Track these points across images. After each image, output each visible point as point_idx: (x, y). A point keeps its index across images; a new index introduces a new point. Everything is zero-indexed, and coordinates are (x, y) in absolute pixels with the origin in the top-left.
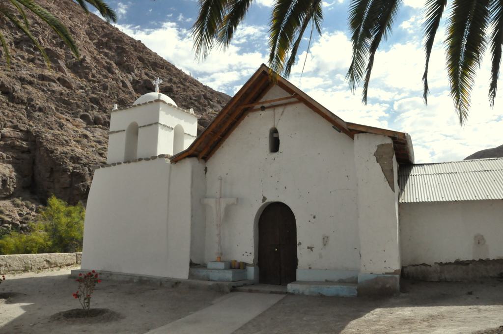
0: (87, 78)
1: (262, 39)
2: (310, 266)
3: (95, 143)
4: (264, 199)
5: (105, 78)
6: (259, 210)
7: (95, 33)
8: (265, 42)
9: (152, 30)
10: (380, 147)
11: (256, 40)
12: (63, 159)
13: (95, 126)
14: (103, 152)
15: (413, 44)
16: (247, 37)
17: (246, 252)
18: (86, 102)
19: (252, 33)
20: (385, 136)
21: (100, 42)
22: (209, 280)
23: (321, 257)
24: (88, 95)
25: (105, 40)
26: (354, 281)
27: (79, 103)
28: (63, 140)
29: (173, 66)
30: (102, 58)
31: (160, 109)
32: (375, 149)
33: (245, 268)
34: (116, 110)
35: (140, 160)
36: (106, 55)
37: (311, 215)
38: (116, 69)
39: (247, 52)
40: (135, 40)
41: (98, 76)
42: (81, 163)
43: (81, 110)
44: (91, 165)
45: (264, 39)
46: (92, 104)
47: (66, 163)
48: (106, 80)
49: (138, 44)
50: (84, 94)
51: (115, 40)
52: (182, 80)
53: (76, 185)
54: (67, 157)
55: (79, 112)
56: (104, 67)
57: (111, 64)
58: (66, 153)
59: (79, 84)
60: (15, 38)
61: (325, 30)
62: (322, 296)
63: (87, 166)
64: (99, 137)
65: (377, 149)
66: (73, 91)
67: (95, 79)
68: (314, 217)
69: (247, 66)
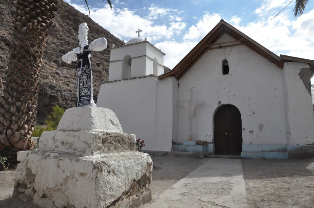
0: (57, 37)
1: (167, 17)
2: (251, 143)
3: (63, 78)
4: (220, 102)
5: (68, 38)
6: (217, 108)
7: (60, 10)
8: (169, 19)
9: (97, 9)
10: (302, 70)
11: (164, 17)
12: (45, 87)
13: (63, 67)
14: (69, 83)
15: (262, 23)
16: (158, 15)
17: (208, 135)
18: (57, 52)
19: (161, 13)
20: (305, 63)
21: (64, 15)
22: (186, 152)
23: (258, 137)
24: (58, 48)
25: (66, 14)
26: (284, 150)
27: (53, 52)
28: (44, 75)
29: (109, 32)
30: (65, 25)
31: (147, 47)
32: (299, 71)
33: (207, 145)
34: (114, 48)
35: (135, 78)
36: (67, 23)
37: (251, 112)
38: (74, 32)
39: (157, 25)
40: (85, 15)
41: (64, 36)
42: (56, 90)
43: (54, 57)
44: (62, 91)
45: (169, 17)
46: (61, 54)
47: (46, 89)
48: (68, 39)
49: (87, 17)
50: (55, 47)
51: (73, 14)
52: (114, 41)
53: (53, 104)
54: (47, 86)
55: (53, 58)
56: (67, 31)
57: (71, 29)
58: (46, 83)
59: (52, 41)
60: (11, 10)
61: (208, 12)
62: (264, 159)
63: (60, 92)
64: (65, 74)
65: (300, 71)
66: (48, 45)
67: (62, 38)
68: (254, 113)
69: (157, 34)
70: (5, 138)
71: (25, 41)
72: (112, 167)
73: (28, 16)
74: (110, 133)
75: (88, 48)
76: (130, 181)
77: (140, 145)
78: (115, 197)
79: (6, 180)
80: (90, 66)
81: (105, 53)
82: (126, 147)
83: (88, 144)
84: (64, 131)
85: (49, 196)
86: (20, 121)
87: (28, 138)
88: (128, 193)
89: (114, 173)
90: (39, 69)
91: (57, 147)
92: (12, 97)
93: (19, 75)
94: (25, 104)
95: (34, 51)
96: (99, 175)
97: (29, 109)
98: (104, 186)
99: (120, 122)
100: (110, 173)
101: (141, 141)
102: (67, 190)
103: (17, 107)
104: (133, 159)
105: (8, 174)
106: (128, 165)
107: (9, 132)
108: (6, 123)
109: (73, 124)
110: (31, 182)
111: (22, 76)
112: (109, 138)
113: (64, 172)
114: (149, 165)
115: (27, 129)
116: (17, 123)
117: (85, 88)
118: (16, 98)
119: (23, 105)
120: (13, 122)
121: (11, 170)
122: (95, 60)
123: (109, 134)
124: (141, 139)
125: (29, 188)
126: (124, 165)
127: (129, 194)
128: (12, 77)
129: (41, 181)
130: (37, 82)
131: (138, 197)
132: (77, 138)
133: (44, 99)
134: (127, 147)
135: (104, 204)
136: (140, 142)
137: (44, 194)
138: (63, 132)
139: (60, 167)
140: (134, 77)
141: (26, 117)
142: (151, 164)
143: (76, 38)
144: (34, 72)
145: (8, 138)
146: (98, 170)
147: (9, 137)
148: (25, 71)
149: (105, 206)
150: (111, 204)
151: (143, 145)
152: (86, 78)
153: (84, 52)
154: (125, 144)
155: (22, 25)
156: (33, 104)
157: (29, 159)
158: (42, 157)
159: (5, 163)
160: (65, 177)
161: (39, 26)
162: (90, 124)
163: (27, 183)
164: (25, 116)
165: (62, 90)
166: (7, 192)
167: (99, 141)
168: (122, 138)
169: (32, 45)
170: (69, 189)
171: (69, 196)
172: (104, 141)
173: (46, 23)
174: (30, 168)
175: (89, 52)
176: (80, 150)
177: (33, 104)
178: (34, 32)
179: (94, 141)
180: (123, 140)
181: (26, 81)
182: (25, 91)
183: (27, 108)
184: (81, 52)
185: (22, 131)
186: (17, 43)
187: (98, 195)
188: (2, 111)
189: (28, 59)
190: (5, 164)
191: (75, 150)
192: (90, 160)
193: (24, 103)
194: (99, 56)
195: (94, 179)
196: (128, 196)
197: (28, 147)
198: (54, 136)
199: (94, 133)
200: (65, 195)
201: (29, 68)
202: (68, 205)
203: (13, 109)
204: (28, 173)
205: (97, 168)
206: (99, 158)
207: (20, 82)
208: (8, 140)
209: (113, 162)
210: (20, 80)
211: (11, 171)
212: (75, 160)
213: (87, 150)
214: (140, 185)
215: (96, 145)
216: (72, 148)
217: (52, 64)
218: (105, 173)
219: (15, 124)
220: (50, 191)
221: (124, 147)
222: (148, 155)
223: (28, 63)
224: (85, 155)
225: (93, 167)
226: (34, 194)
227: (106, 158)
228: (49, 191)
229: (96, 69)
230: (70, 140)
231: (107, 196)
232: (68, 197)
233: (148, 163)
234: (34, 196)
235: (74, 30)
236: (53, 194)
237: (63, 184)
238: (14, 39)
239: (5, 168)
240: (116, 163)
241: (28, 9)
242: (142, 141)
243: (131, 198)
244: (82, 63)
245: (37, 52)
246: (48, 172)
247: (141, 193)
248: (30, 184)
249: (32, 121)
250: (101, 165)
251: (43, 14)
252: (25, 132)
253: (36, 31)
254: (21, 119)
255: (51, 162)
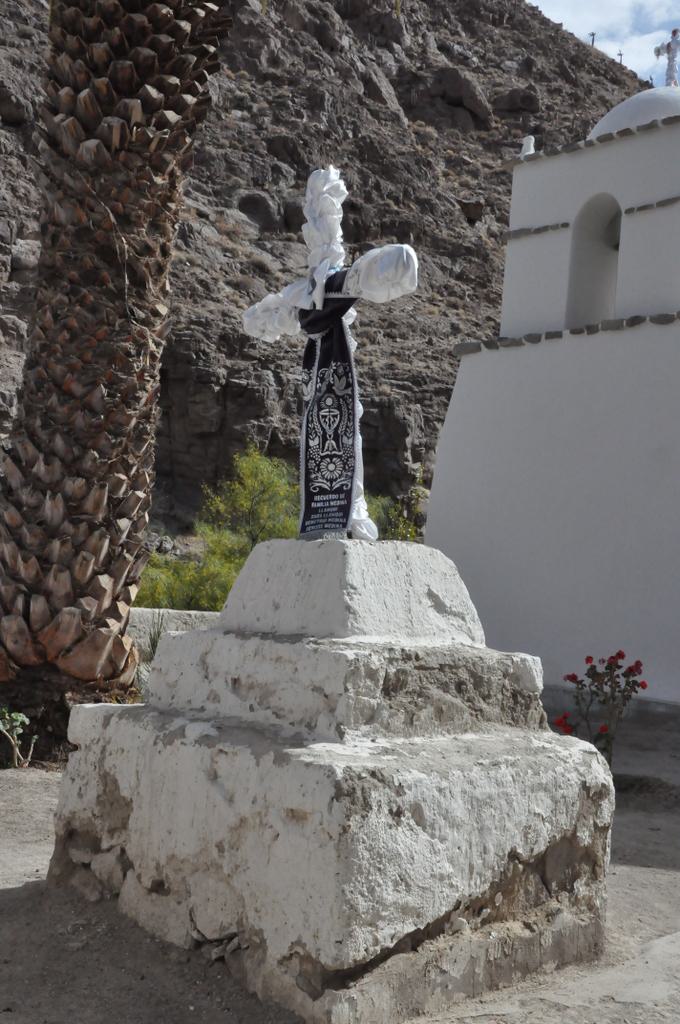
0: (253, 69)
12: (199, 341)
18: (257, 153)
28: (193, 280)
34: (530, 158)
35: (635, 321)
41: (288, 60)
47: (204, 353)
48: (313, 73)
53: (238, 427)
54: (208, 337)
55: (237, 186)
56: (305, 27)
57: (326, 15)
58: (207, 324)
59: (230, 90)
63: (272, 367)
67: (278, 72)
70: (21, 632)
71: (92, 202)
72: (410, 796)
73: (101, 82)
74: (421, 654)
75: (344, 288)
76: (491, 858)
77: (622, 681)
78: (418, 917)
79: (22, 810)
80: (350, 365)
81: (510, 140)
82: (492, 710)
83: (326, 696)
84: (242, 634)
85: (175, 887)
86: (80, 558)
87: (111, 632)
88: (481, 909)
89: (420, 820)
90: (158, 328)
91: (214, 697)
92: (50, 455)
93: (74, 360)
94: (103, 487)
95: (134, 248)
96: (354, 822)
97: (115, 506)
98: (372, 869)
99: (473, 602)
100: (403, 819)
101: (625, 664)
102: (240, 869)
103: (67, 499)
104: (513, 765)
105: (32, 783)
106: (486, 788)
107: (38, 605)
108: (26, 569)
109: (277, 607)
110: (113, 827)
111: (85, 362)
112: (416, 671)
113: (231, 800)
114: (592, 795)
115: (109, 591)
116: (69, 567)
117: (331, 457)
118: (62, 460)
119: (92, 492)
120: (52, 564)
121: (43, 767)
122: (453, 190)
123: (417, 658)
124: (626, 658)
125: (109, 850)
126: (468, 787)
127: (487, 911)
128: (46, 367)
129: (149, 828)
130: (148, 387)
131: (533, 931)
132: (289, 668)
133: (195, 402)
134: (497, 710)
135: (370, 937)
136: (623, 670)
137: (157, 878)
138: (239, 641)
139: (219, 780)
140: (628, 316)
141: (107, 543)
142: (602, 792)
143: (353, 64)
144: (135, 342)
145: (33, 634)
146: (353, 803)
147: (36, 627)
148: (99, 340)
149: (371, 949)
150: (400, 941)
151: (635, 682)
152: (336, 416)
153: (326, 302)
154: (485, 698)
155: (80, 128)
156: (135, 484)
157: (110, 738)
158: (157, 737)
159: (20, 737)
160: (233, 820)
161: (153, 128)
162: (341, 617)
163: (102, 830)
164: (102, 537)
165: (284, 358)
166: (31, 862)
167: (367, 687)
168: (473, 674)
169: (126, 221)
170: (248, 868)
171: (246, 894)
172: (391, 688)
173: (180, 107)
174: (112, 773)
175: (349, 303)
176: (297, 717)
177: (135, 484)
178: (131, 155)
179: (349, 686)
180: (478, 682)
181: (105, 387)
182: (99, 428)
183: (108, 504)
184: (314, 305)
185: (89, 604)
186: (62, 214)
187: (347, 902)
188: (11, 515)
189: (111, 285)
190: (20, 742)
191: (278, 716)
192: (326, 761)
193: (95, 480)
194: (477, 163)
195: (335, 836)
196: (484, 922)
197: (110, 671)
198: (206, 654)
199: (350, 654)
200: (232, 889)
201: (114, 325)
202: (241, 929)
203: (52, 509)
204: (104, 791)
205: (348, 795)
206: (365, 754)
207: (77, 389)
208: (35, 641)
209: (417, 774)
210: (78, 380)
211: (43, 772)
212: (272, 758)
213: (322, 721)
214: (545, 882)
215: (357, 701)
216: (269, 708)
217: (232, 221)
218: (379, 819)
219: (61, 571)
220: (180, 870)
221: (481, 710)
222: (591, 753)
223: (111, 305)
224: (315, 741)
225: (332, 791)
226: (125, 875)
227: (389, 757)
228: (178, 871)
229: (459, 236)
230: (265, 673)
231: (386, 907)
232: (241, 899)
233: (585, 786)
234: (122, 884)
235: (343, 17)
236: (191, 881)
237: (226, 847)
238: (49, 196)
239: (19, 759)
240: (430, 781)
241: (99, 49)
242: (632, 664)
243: (497, 931)
244: (318, 352)
245: (148, 250)
246: (174, 793)
247: (547, 916)
248: (112, 837)
249: (128, 562)
250: (366, 785)
251: (168, 66)
252: (100, 606)
253: (139, 153)
254: (84, 553)
255: (187, 758)
